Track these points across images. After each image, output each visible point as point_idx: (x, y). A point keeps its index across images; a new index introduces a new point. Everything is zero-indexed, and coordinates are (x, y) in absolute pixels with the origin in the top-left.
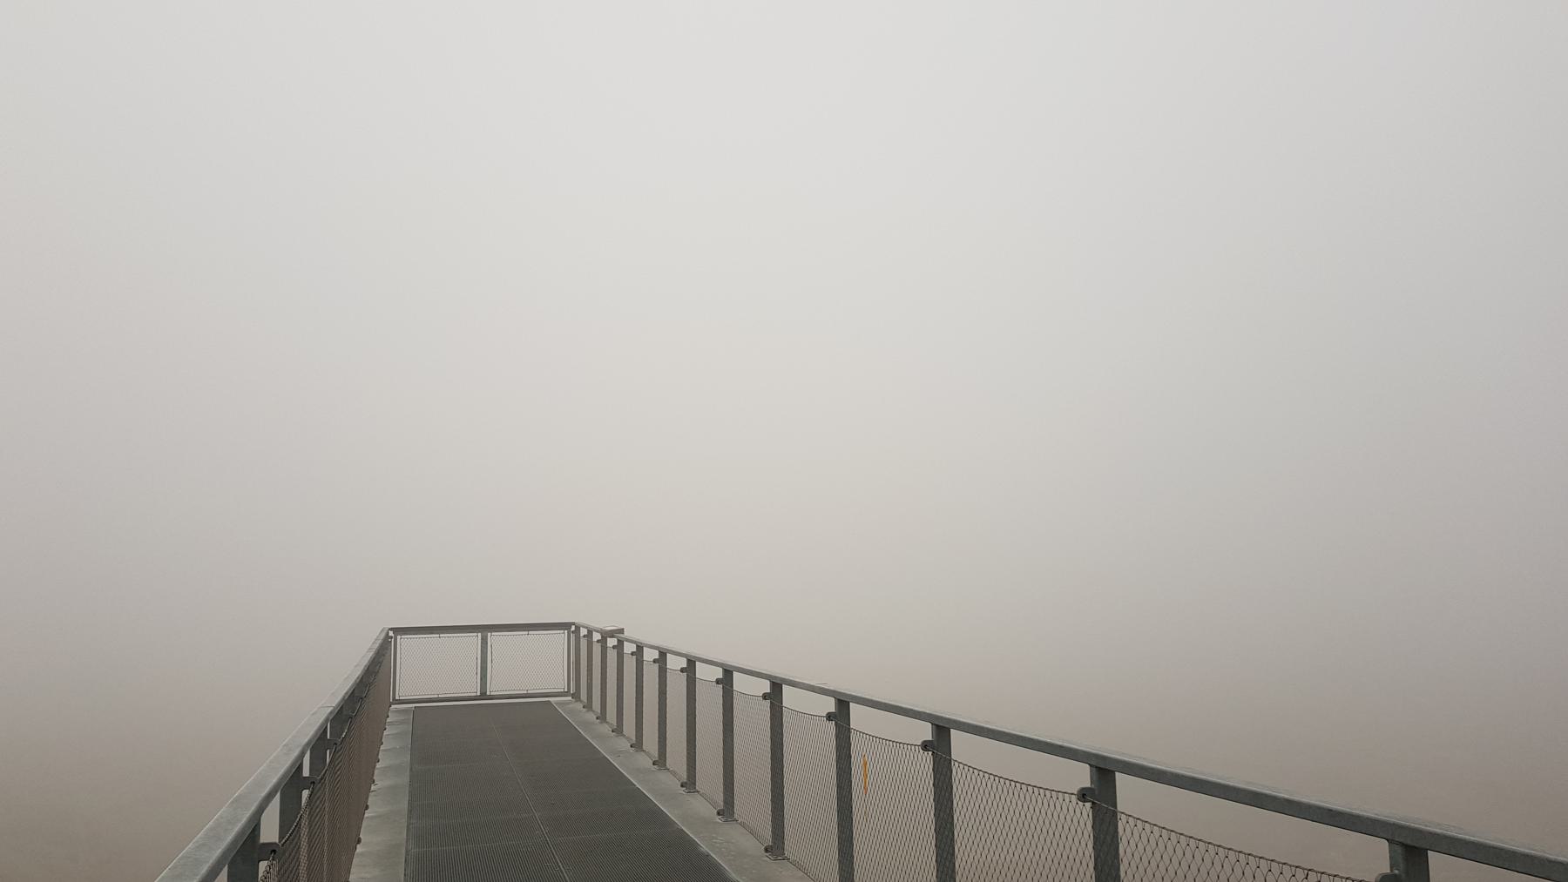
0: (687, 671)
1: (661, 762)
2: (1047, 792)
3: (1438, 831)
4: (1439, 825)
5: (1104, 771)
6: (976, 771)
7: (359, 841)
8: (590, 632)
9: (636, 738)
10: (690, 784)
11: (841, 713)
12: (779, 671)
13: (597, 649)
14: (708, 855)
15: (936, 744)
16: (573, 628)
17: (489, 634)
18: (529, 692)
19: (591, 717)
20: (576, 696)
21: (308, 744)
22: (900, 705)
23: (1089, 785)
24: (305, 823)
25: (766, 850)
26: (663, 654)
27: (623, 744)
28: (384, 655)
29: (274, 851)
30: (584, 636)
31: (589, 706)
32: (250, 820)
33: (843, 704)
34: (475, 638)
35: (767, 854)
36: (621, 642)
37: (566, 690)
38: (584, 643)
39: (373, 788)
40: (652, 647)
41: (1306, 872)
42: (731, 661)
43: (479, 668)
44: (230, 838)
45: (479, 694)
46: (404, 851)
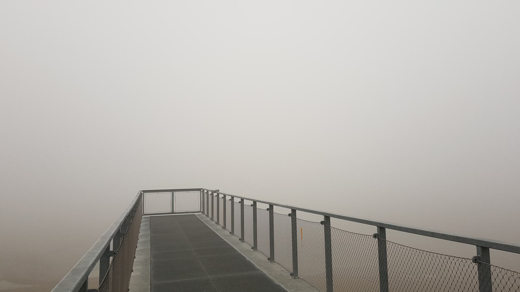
0: (269, 210)
1: (232, 232)
2: (359, 235)
3: (493, 242)
4: (493, 240)
5: (382, 228)
6: (343, 231)
7: (135, 257)
8: (208, 191)
9: (224, 225)
10: (242, 239)
11: (271, 208)
12: (272, 201)
13: (210, 197)
14: (249, 261)
15: (325, 222)
16: (202, 190)
17: (174, 192)
18: (188, 211)
19: (208, 219)
20: (203, 212)
21: (112, 236)
22: (313, 210)
23: (377, 233)
24: (111, 272)
25: (268, 259)
26: (233, 197)
27: (219, 227)
28: (141, 199)
29: (115, 253)
30: (206, 193)
31: (207, 216)
32: (83, 278)
33: (294, 210)
34: (169, 194)
35: (269, 261)
36: (218, 194)
37: (200, 211)
38: (206, 195)
39: (138, 241)
40: (205, 190)
41: (449, 257)
42: (256, 198)
43: (171, 204)
44: (103, 247)
45: (171, 212)
46: (150, 261)
